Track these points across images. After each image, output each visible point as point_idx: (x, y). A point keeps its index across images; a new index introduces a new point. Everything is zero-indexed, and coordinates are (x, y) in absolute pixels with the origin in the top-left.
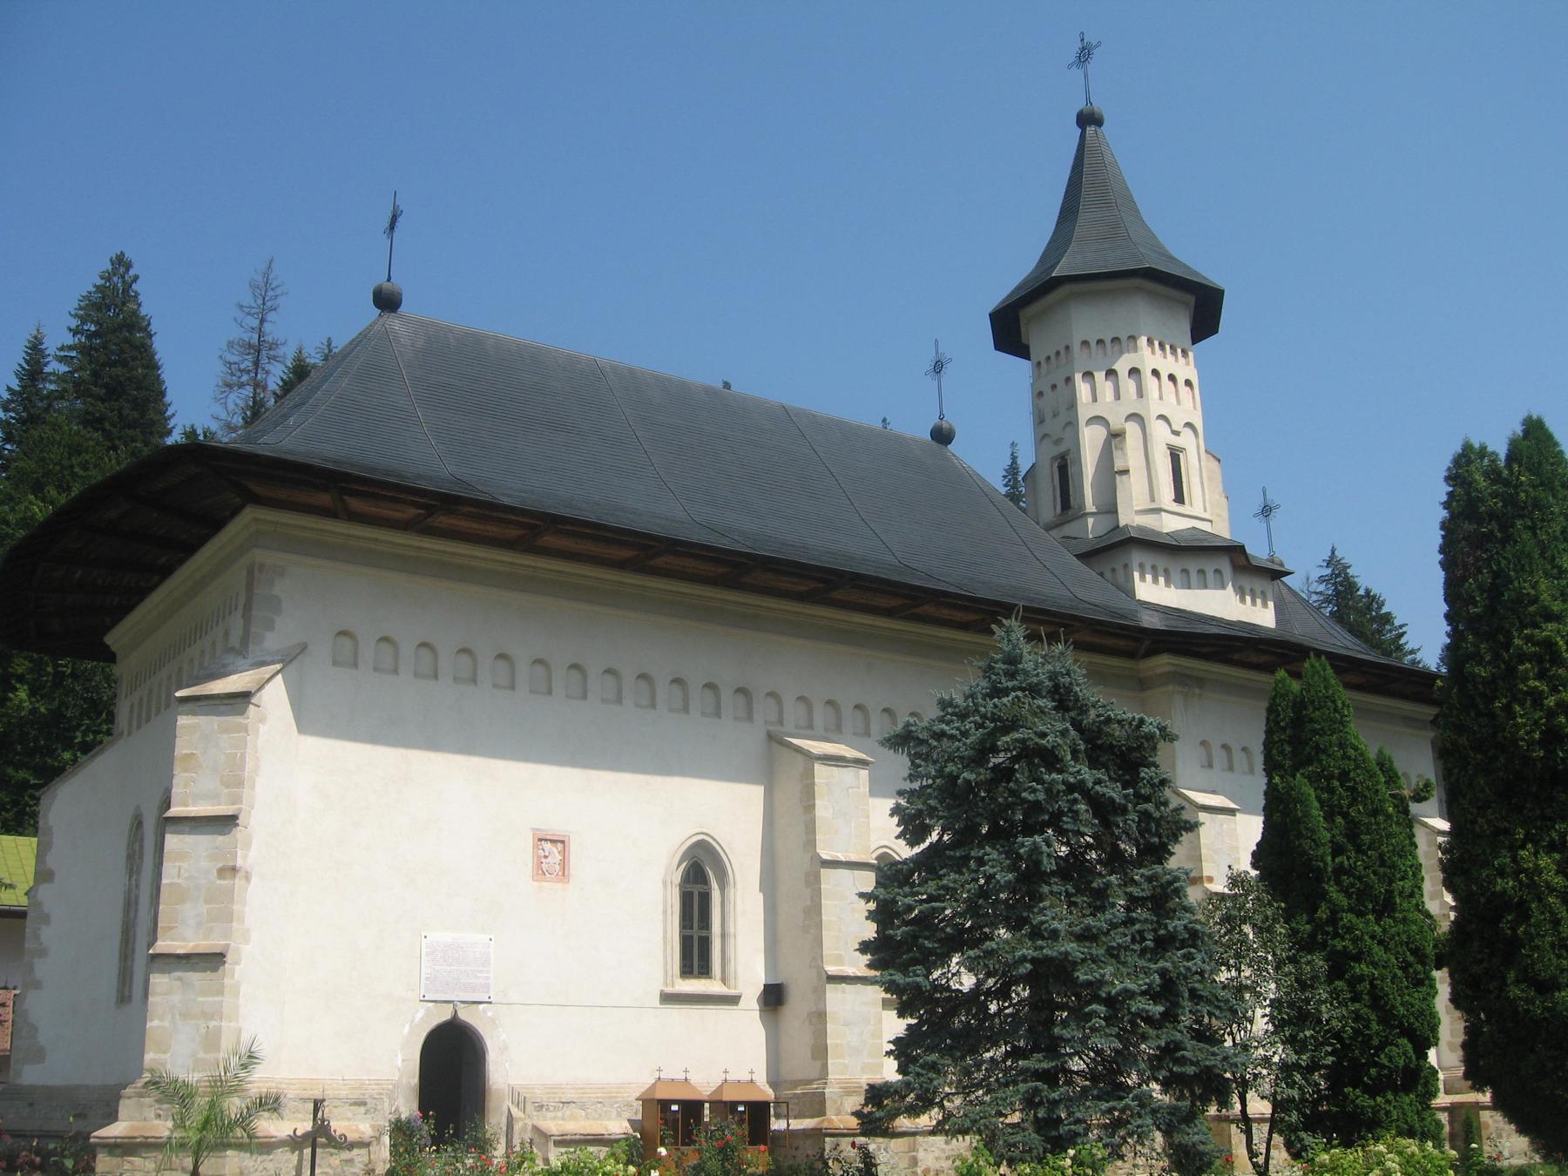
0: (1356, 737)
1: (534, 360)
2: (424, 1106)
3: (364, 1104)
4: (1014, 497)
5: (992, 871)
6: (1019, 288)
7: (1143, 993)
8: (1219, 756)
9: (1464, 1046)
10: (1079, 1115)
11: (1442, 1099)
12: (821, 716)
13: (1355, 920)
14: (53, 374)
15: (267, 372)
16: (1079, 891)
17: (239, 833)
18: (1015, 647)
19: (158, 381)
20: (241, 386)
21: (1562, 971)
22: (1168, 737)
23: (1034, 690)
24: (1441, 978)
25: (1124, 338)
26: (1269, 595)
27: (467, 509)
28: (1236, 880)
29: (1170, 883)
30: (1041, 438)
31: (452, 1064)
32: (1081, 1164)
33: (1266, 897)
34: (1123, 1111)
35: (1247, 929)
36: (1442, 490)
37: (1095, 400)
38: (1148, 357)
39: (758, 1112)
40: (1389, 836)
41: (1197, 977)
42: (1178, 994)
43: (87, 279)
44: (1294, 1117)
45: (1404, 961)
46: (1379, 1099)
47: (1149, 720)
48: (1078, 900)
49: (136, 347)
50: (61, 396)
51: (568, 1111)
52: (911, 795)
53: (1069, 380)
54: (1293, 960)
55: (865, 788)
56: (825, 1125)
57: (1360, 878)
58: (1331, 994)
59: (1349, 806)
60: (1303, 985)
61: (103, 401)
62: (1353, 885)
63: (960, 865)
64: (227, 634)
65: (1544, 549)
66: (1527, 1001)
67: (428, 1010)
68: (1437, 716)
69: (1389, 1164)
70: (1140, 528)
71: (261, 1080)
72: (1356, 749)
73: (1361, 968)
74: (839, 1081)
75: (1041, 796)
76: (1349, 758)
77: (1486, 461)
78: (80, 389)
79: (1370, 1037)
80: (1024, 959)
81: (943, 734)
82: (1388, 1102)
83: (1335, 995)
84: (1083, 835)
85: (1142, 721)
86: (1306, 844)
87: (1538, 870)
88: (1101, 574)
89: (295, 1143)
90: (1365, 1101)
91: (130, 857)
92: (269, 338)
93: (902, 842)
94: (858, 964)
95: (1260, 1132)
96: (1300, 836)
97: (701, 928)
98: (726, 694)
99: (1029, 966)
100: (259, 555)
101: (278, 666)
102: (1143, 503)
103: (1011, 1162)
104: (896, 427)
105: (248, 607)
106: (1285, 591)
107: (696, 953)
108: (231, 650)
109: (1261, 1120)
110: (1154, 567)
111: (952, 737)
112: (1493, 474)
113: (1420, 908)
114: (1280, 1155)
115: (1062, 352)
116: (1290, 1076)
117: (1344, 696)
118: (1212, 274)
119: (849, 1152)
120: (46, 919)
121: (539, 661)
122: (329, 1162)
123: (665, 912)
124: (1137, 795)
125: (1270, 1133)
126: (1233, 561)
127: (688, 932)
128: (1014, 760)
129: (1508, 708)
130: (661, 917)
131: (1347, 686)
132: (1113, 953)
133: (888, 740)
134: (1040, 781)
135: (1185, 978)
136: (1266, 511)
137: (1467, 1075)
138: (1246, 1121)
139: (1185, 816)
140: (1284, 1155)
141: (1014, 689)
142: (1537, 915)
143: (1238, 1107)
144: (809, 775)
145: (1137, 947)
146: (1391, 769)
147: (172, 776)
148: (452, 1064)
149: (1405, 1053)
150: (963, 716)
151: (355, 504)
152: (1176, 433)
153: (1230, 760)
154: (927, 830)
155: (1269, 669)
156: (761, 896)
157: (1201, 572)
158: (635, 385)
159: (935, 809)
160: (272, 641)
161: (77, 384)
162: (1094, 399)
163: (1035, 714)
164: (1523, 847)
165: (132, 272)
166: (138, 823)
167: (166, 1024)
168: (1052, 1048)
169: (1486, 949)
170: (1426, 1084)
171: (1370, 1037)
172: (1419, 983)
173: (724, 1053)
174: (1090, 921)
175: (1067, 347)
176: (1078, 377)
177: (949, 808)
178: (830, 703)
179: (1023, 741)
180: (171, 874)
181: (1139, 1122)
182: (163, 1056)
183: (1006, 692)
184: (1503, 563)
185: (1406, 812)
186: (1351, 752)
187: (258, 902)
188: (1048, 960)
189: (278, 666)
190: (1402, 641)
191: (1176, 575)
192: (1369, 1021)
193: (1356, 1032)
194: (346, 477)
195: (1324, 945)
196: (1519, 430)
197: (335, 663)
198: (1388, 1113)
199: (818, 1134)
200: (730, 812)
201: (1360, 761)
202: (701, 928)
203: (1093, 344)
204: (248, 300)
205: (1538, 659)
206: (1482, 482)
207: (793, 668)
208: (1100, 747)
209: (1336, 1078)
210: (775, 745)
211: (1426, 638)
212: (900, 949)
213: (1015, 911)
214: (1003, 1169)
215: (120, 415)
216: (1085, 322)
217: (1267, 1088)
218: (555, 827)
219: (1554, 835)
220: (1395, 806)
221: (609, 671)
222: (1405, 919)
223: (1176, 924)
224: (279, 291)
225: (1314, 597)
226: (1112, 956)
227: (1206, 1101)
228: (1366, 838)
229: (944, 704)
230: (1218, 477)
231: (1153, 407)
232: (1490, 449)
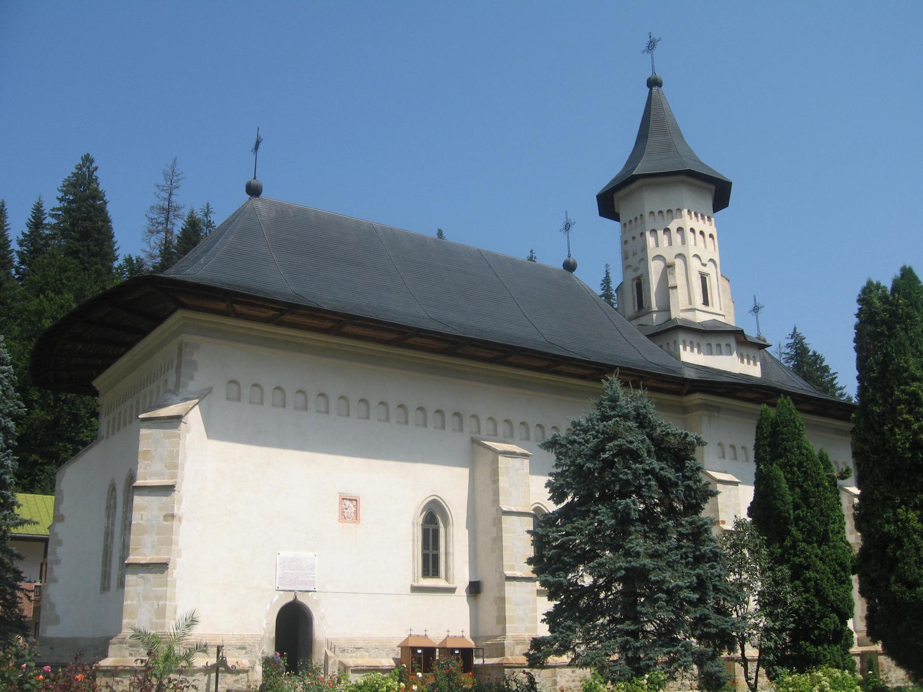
0: (807, 443)
1: (339, 223)
2: (277, 649)
3: (245, 648)
4: (607, 296)
5: (602, 519)
6: (614, 180)
7: (687, 587)
8: (728, 450)
9: (867, 618)
10: (651, 655)
11: (855, 649)
12: (502, 428)
13: (806, 547)
14: (49, 224)
15: (174, 224)
16: (651, 530)
17: (175, 495)
18: (615, 392)
19: (110, 229)
20: (158, 232)
21: (921, 576)
22: (700, 443)
23: (626, 417)
24: (854, 578)
25: (674, 210)
26: (758, 358)
27: (302, 311)
28: (739, 524)
29: (702, 526)
30: (626, 268)
31: (294, 625)
33: (756, 533)
34: (675, 653)
35: (745, 551)
36: (855, 307)
37: (657, 246)
38: (688, 221)
39: (467, 654)
40: (826, 499)
41: (717, 578)
42: (707, 588)
43: (68, 170)
44: (771, 657)
46: (819, 648)
47: (690, 434)
49: (97, 210)
50: (53, 237)
51: (359, 653)
52: (556, 475)
53: (642, 234)
54: (771, 569)
56: (505, 661)
57: (809, 523)
58: (792, 588)
59: (804, 481)
60: (777, 583)
61: (78, 241)
62: (805, 527)
64: (166, 381)
65: (912, 340)
66: (902, 593)
67: (280, 595)
69: (823, 682)
71: (198, 633)
72: (807, 449)
73: (810, 574)
74: (513, 637)
75: (630, 477)
76: (803, 455)
78: (64, 233)
79: (815, 613)
80: (620, 568)
81: (575, 441)
82: (825, 649)
83: (795, 588)
84: (653, 498)
85: (686, 435)
86: (779, 503)
87: (908, 520)
88: (661, 346)
89: (207, 670)
90: (812, 649)
91: (108, 508)
92: (174, 204)
93: (551, 502)
94: (527, 570)
95: (752, 667)
96: (775, 499)
98: (448, 416)
99: (623, 572)
100: (186, 337)
101: (197, 401)
102: (685, 306)
103: (613, 682)
104: (541, 260)
105: (179, 367)
106: (766, 356)
107: (431, 564)
108: (169, 391)
109: (752, 660)
110: (691, 343)
111: (580, 443)
112: (884, 299)
113: (843, 539)
114: (763, 680)
115: (639, 218)
116: (769, 634)
117: (800, 418)
118: (723, 170)
119: (521, 676)
120: (60, 543)
121: (342, 398)
122: (227, 681)
123: (413, 540)
124: (684, 476)
125: (758, 667)
126: (737, 339)
127: (427, 552)
128: (614, 456)
129: (891, 430)
130: (411, 543)
132: (670, 565)
134: (629, 468)
135: (711, 579)
136: (756, 309)
137: (869, 633)
138: (744, 661)
139: (710, 487)
140: (766, 679)
141: (614, 416)
142: (907, 545)
143: (740, 652)
144: (496, 462)
145: (683, 561)
147: (137, 463)
148: (294, 625)
150: (585, 431)
151: (238, 308)
152: (704, 265)
153: (735, 454)
154: (565, 496)
155: (758, 401)
158: (395, 238)
159: (570, 483)
160: (193, 386)
161: (64, 230)
162: (657, 246)
163: (627, 430)
164: (899, 507)
165: (94, 165)
166: (113, 488)
167: (135, 603)
168: (636, 619)
169: (878, 564)
170: (846, 639)
171: (815, 613)
172: (842, 582)
173: (446, 621)
174: (657, 547)
177: (578, 483)
179: (620, 446)
180: (136, 518)
181: (685, 659)
182: (134, 621)
184: (889, 349)
185: (835, 485)
186: (805, 451)
189: (197, 401)
190: (835, 382)
191: (704, 347)
192: (814, 603)
193: (807, 610)
194: (236, 294)
195: (788, 561)
196: (898, 274)
197: (228, 399)
198: (824, 656)
199: (500, 667)
200: (450, 483)
201: (809, 457)
204: (162, 182)
205: (909, 403)
206: (878, 304)
207: (485, 401)
208: (663, 449)
209: (795, 635)
211: (848, 383)
212: (550, 561)
213: (614, 540)
214: (609, 685)
215: (88, 250)
216: (651, 201)
217: (756, 641)
218: (352, 492)
219: (917, 501)
220: (829, 482)
222: (834, 546)
224: (180, 177)
225: (784, 356)
226: (670, 566)
227: (722, 648)
228: (813, 500)
229: (575, 424)
231: (691, 250)
232: (882, 285)
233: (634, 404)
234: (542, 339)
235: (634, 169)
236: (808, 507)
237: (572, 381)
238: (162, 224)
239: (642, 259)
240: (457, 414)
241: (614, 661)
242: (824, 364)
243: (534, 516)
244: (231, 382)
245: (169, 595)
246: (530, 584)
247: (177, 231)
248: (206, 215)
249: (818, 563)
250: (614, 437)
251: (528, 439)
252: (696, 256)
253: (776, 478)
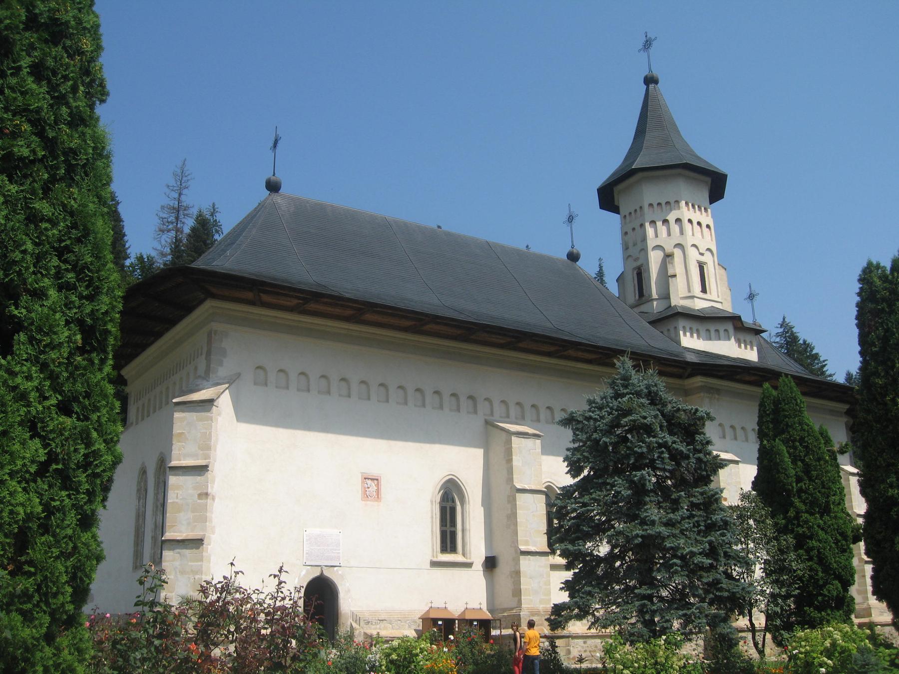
1: (353, 217)
7: (700, 554)
8: (729, 431)
12: (514, 411)
13: (809, 517)
17: (209, 475)
18: (627, 371)
20: (169, 231)
23: (638, 394)
25: (672, 202)
26: (754, 343)
27: (326, 300)
28: (849, 376)
29: (713, 495)
30: (627, 258)
32: (669, 643)
36: (857, 286)
37: (657, 236)
38: (686, 212)
39: (485, 624)
40: (827, 472)
42: (718, 555)
44: (778, 622)
45: (836, 539)
46: (823, 613)
48: (664, 505)
51: (382, 625)
53: (642, 225)
54: (776, 538)
55: (539, 450)
57: (811, 495)
59: (805, 456)
60: (781, 551)
62: (807, 498)
63: (600, 487)
64: (196, 368)
68: (848, 410)
69: (835, 636)
70: (682, 307)
72: (808, 425)
75: (645, 450)
76: (804, 430)
77: (880, 271)
79: (818, 580)
80: (637, 536)
81: (591, 418)
82: (828, 615)
85: (697, 410)
90: (815, 614)
96: (778, 472)
98: (463, 399)
99: (640, 539)
100: (215, 326)
101: (227, 385)
102: (684, 293)
103: (632, 643)
105: (209, 354)
106: (762, 341)
107: (449, 540)
108: (200, 377)
110: (691, 329)
111: (596, 420)
112: (884, 278)
117: (801, 398)
118: (718, 164)
121: (363, 382)
123: (432, 517)
124: (695, 449)
126: (735, 325)
127: (444, 528)
128: (627, 432)
130: (430, 520)
131: (804, 394)
133: (561, 421)
135: (722, 546)
136: (751, 297)
138: (752, 629)
141: (628, 394)
144: (509, 442)
145: (696, 529)
146: (827, 436)
149: (837, 589)
150: (600, 408)
151: (265, 298)
152: (702, 254)
154: (581, 470)
156: (482, 508)
157: (717, 331)
158: (407, 231)
159: (587, 458)
160: (222, 372)
162: (656, 236)
163: (640, 407)
166: (144, 472)
169: (879, 530)
170: (848, 606)
171: (818, 580)
173: (464, 593)
175: (641, 207)
176: (647, 225)
177: (594, 457)
178: (518, 404)
179: (634, 421)
180: (172, 497)
183: (623, 395)
184: (890, 324)
185: (836, 459)
187: (218, 510)
188: (650, 536)
189: (227, 385)
191: (703, 333)
192: (817, 571)
193: (811, 577)
194: (263, 283)
195: (792, 531)
197: (255, 384)
200: (466, 463)
203: (655, 206)
204: (172, 182)
206: (878, 282)
207: (497, 385)
208: (673, 424)
209: (799, 601)
210: (490, 427)
216: (650, 193)
218: (374, 471)
220: (830, 456)
223: (716, 517)
224: (189, 177)
226: (683, 534)
228: (814, 473)
229: (590, 402)
230: (725, 278)
231: (689, 240)
232: (882, 265)
233: (646, 382)
234: (549, 325)
235: (633, 163)
236: (810, 479)
238: (172, 223)
239: (642, 249)
240: (471, 397)
241: (632, 624)
242: (814, 352)
243: (547, 496)
244: (258, 368)
245: (204, 569)
246: (543, 558)
247: (187, 230)
248: (212, 215)
249: (820, 532)
250: (628, 412)
251: (538, 420)
252: (694, 245)
253: (779, 453)
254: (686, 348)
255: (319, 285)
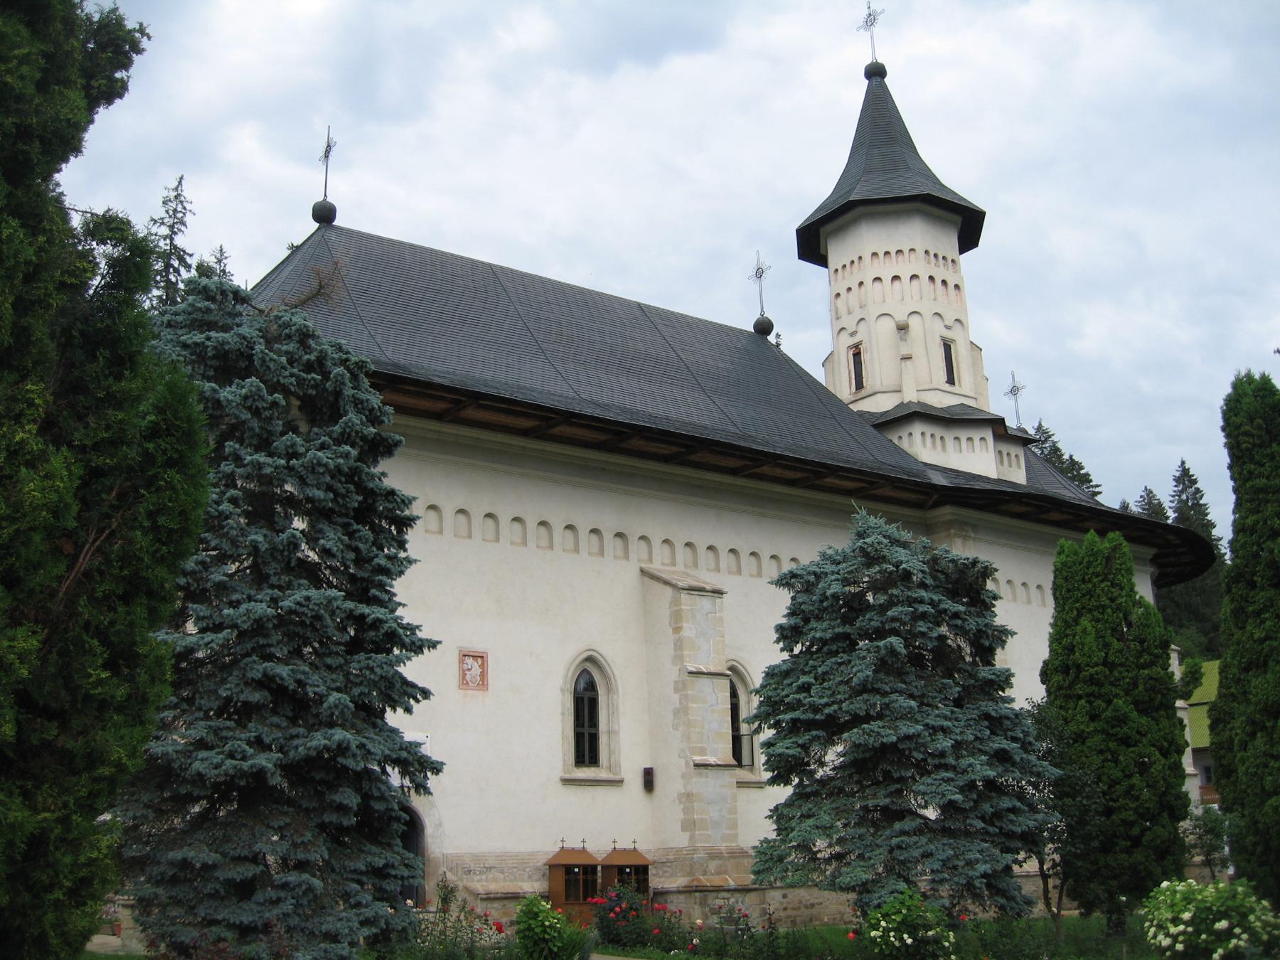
51: (494, 873)
74: (705, 848)
97: (591, 726)
98: (608, 537)
107: (586, 747)
118: (976, 198)
121: (461, 511)
175: (860, 258)
202: (591, 726)
203: (893, 254)
218: (477, 646)
221: (516, 519)
234: (733, 429)
235: (849, 192)
237: (779, 488)
248: (219, 261)
254: (926, 464)
255: (396, 365)
